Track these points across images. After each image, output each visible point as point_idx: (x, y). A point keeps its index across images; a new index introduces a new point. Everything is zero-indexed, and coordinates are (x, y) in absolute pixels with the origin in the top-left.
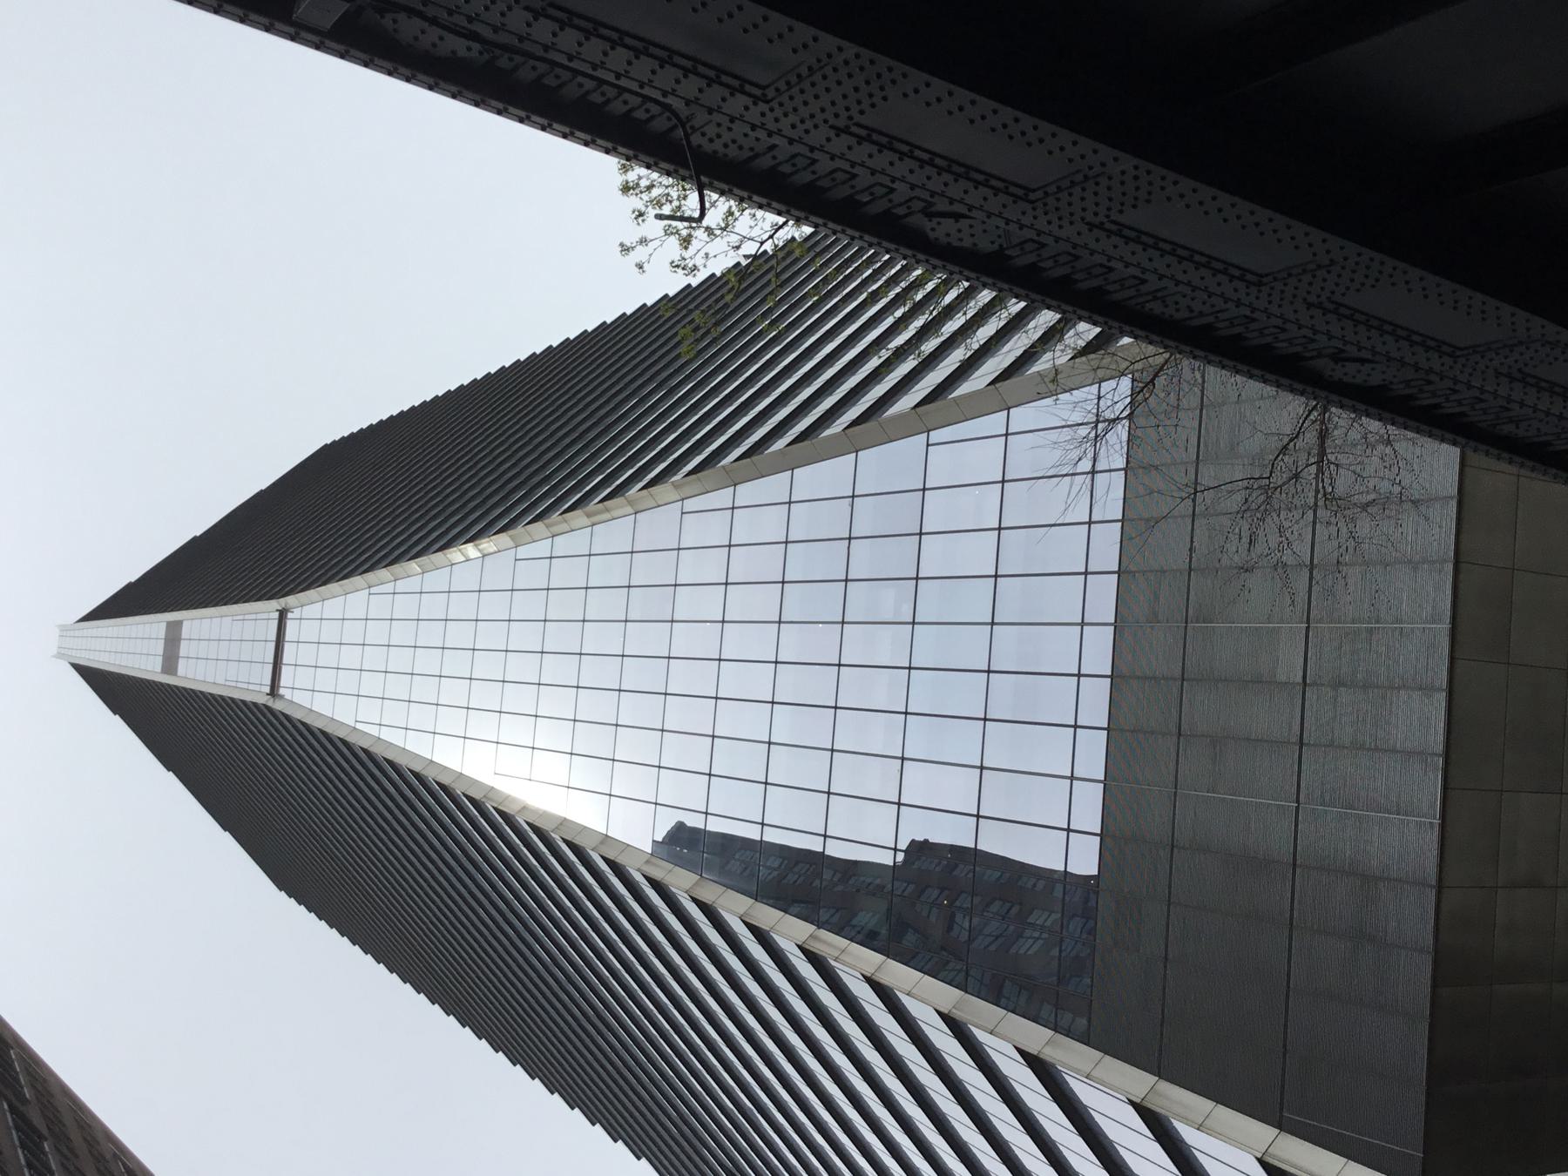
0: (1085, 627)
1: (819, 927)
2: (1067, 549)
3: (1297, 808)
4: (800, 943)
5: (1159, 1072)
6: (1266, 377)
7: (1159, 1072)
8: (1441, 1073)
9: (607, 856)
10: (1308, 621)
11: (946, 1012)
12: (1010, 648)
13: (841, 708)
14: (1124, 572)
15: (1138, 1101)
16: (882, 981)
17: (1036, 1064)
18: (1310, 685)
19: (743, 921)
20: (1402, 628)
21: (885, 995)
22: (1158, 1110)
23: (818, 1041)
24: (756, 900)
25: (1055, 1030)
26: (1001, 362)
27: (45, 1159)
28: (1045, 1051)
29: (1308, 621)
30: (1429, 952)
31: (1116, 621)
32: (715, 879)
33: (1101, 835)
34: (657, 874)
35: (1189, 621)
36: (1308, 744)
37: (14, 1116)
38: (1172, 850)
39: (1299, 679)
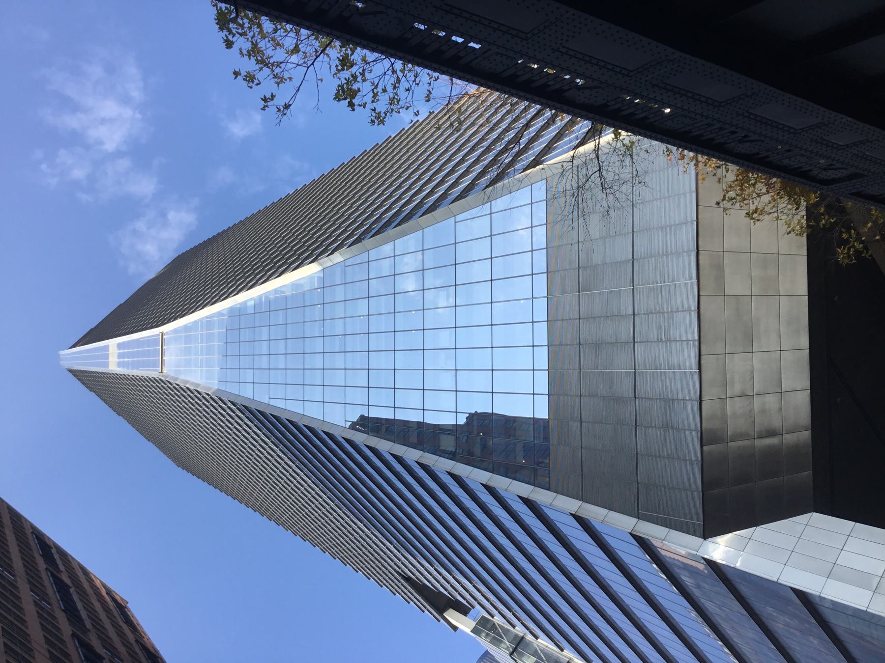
0: (534, 300)
1: (424, 452)
2: (523, 334)
3: (635, 372)
4: (416, 460)
5: (582, 499)
6: (608, 122)
7: (582, 499)
8: (707, 485)
9: (521, 495)
10: (633, 286)
11: (485, 483)
12: (501, 336)
13: (453, 349)
14: (551, 345)
15: (449, 471)
16: (455, 473)
17: (584, 523)
18: (637, 315)
19: (390, 453)
20: (675, 284)
21: (584, 523)
22: (584, 516)
23: (429, 520)
24: (457, 462)
25: (535, 486)
26: (502, 560)
27: (84, 650)
28: (531, 495)
29: (633, 286)
30: (699, 461)
31: (548, 369)
32: (376, 435)
33: (549, 395)
34: (348, 437)
35: (582, 367)
36: (638, 342)
37: (64, 602)
38: (581, 397)
39: (631, 312)
